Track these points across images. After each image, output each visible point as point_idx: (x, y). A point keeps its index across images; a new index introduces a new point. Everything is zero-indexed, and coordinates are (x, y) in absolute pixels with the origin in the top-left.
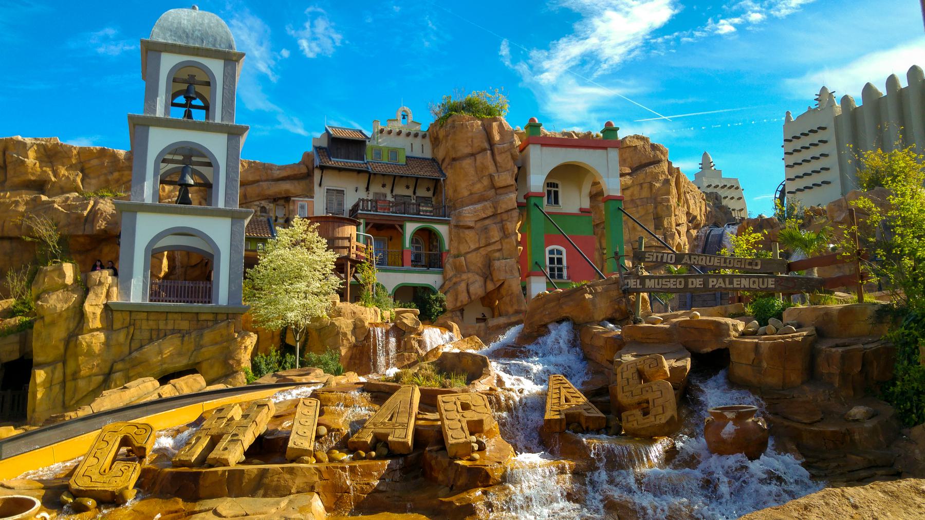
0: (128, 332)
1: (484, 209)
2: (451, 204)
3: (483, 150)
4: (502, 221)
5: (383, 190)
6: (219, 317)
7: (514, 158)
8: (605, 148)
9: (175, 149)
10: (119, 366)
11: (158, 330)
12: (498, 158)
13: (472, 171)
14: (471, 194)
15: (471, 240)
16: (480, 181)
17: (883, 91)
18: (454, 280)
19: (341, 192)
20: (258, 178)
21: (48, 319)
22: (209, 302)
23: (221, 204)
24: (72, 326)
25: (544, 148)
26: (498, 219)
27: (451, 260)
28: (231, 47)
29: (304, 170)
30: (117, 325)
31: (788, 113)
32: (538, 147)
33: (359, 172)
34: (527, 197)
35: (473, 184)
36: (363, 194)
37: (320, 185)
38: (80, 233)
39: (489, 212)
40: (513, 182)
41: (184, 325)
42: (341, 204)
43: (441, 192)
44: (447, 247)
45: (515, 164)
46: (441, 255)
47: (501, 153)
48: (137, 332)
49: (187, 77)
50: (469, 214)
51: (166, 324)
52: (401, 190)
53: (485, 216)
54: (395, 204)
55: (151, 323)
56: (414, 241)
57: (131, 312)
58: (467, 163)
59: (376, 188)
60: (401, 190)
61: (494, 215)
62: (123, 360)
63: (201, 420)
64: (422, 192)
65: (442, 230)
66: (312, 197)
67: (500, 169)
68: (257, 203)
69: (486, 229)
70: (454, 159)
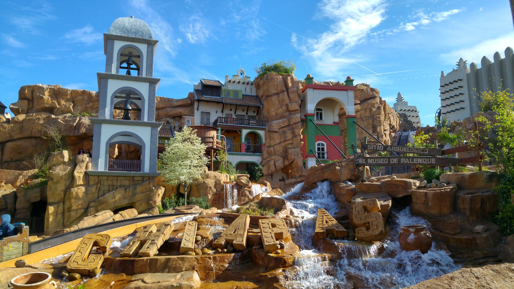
0: (97, 187)
1: (283, 122)
3: (283, 91)
6: (145, 179)
8: (347, 90)
9: (122, 91)
10: (92, 204)
11: (113, 185)
12: (291, 96)
13: (277, 102)
14: (277, 114)
16: (281, 107)
17: (492, 60)
18: (268, 159)
20: (165, 106)
21: (55, 180)
23: (146, 120)
24: (68, 183)
25: (315, 91)
26: (291, 127)
27: (266, 149)
28: (151, 37)
30: (91, 183)
31: (442, 72)
32: (312, 90)
33: (218, 103)
34: (306, 116)
35: (278, 109)
36: (220, 114)
37: (198, 110)
38: (72, 135)
39: (286, 124)
40: (299, 108)
41: (127, 183)
42: (208, 119)
44: (264, 142)
45: (299, 99)
48: (102, 187)
49: (128, 53)
50: (276, 125)
51: (117, 182)
53: (284, 126)
55: (109, 182)
57: (98, 176)
58: (274, 98)
59: (227, 111)
61: (289, 125)
63: (135, 232)
64: (251, 113)
65: (262, 133)
66: (193, 116)
68: (165, 119)
69: (284, 133)
70: (268, 96)
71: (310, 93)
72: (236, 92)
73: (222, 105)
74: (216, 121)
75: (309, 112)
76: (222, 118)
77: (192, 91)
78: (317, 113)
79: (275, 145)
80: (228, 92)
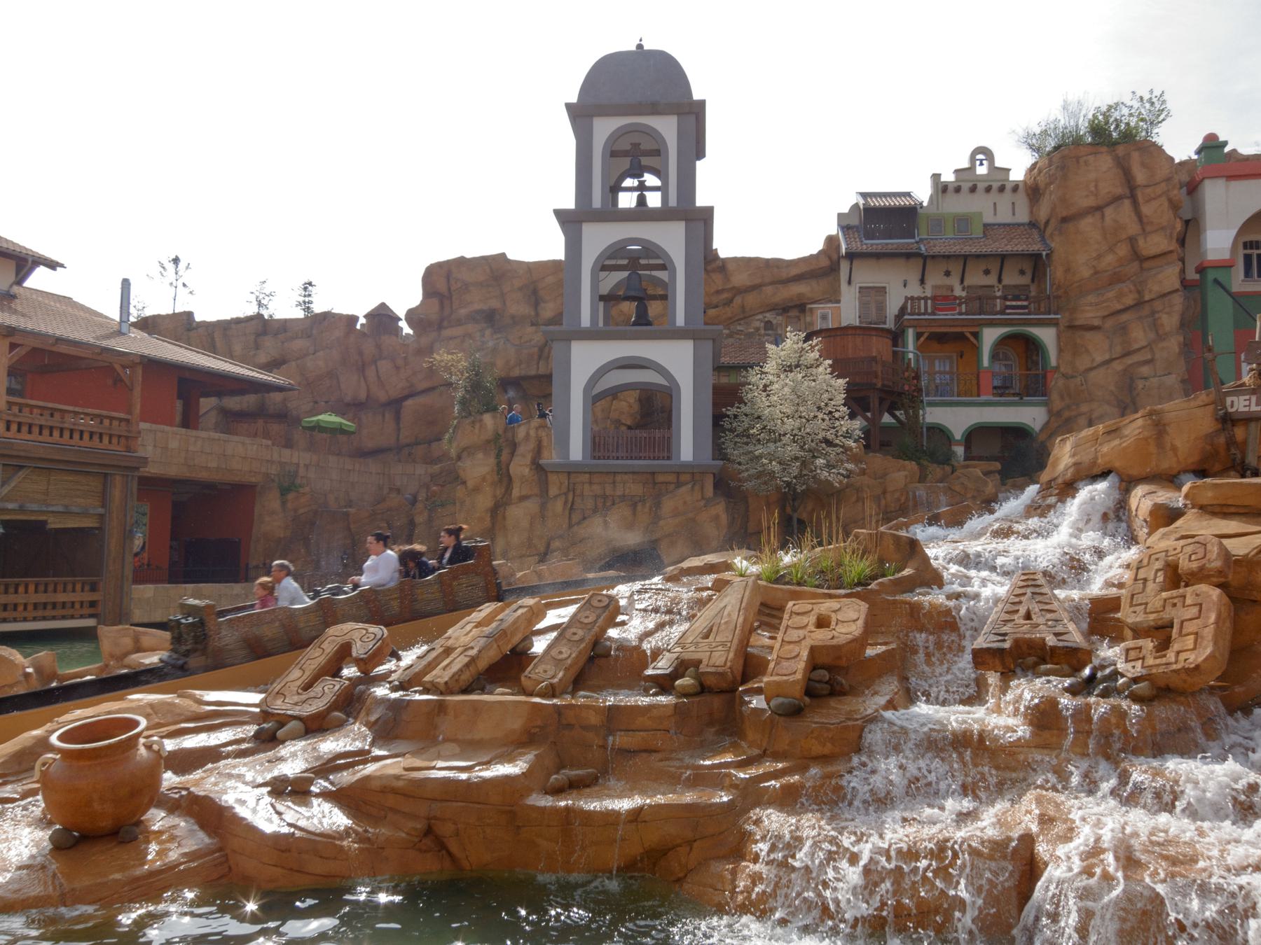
0: (566, 502)
2: (1060, 293)
3: (1117, 199)
4: (1153, 313)
5: (947, 281)
6: (683, 478)
7: (1175, 206)
9: (617, 250)
11: (605, 497)
12: (1146, 210)
14: (1096, 273)
15: (1098, 348)
16: (1111, 249)
18: (1066, 414)
19: (882, 290)
20: (758, 281)
21: (470, 484)
22: (669, 458)
24: (499, 492)
25: (1237, 185)
26: (1146, 310)
27: (1061, 382)
29: (825, 262)
30: (553, 491)
32: (1221, 183)
33: (908, 256)
34: (1201, 270)
35: (1099, 257)
36: (915, 290)
37: (849, 282)
38: (533, 373)
39: (1129, 300)
40: (1174, 246)
42: (881, 307)
43: (1045, 275)
45: (1176, 215)
46: (1045, 377)
47: (1148, 201)
48: (578, 500)
49: (628, 147)
52: (976, 278)
53: (1119, 307)
54: (968, 300)
56: (994, 356)
57: (569, 473)
58: (1087, 224)
59: (936, 279)
60: (976, 278)
61: (1139, 304)
62: (561, 537)
64: (1012, 278)
65: (1047, 336)
66: (838, 301)
67: (1148, 228)
68: (760, 317)
69: (1123, 329)
70: (1065, 220)
71: (1215, 194)
72: (963, 222)
73: (921, 261)
74: (903, 310)
75: (1211, 256)
76: (926, 299)
77: (833, 229)
78: (1248, 258)
79: (1091, 369)
80: (938, 222)
